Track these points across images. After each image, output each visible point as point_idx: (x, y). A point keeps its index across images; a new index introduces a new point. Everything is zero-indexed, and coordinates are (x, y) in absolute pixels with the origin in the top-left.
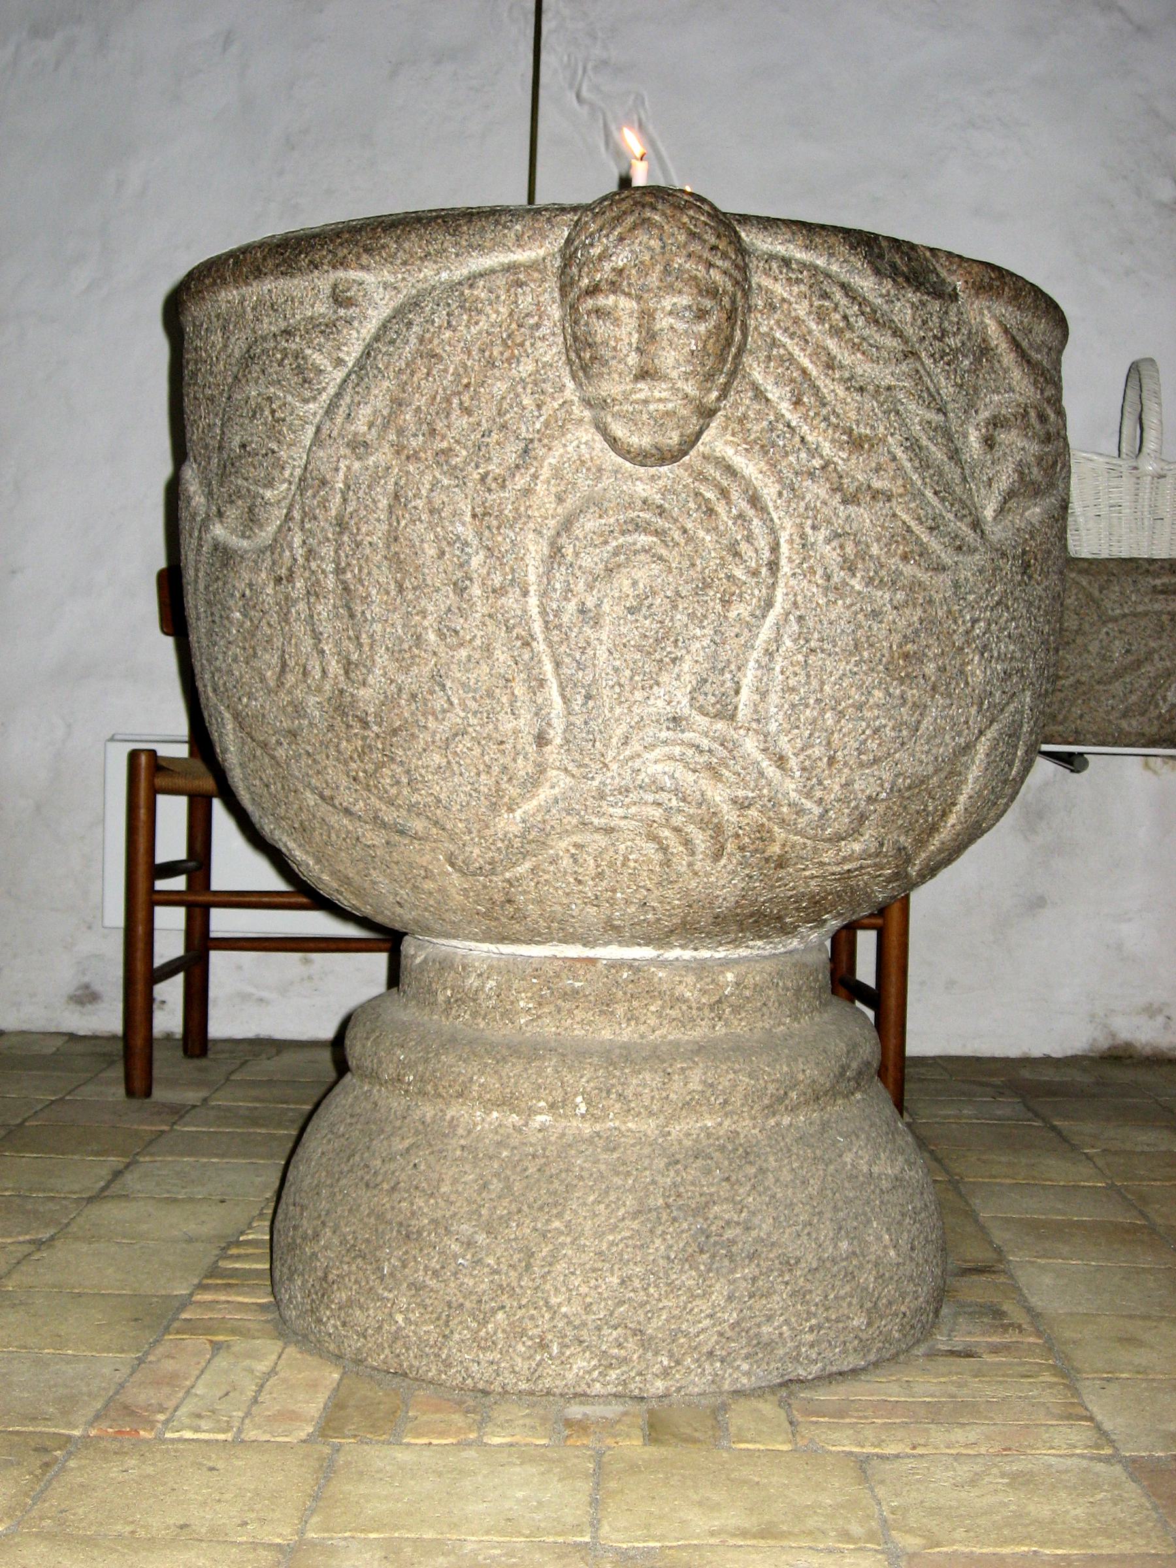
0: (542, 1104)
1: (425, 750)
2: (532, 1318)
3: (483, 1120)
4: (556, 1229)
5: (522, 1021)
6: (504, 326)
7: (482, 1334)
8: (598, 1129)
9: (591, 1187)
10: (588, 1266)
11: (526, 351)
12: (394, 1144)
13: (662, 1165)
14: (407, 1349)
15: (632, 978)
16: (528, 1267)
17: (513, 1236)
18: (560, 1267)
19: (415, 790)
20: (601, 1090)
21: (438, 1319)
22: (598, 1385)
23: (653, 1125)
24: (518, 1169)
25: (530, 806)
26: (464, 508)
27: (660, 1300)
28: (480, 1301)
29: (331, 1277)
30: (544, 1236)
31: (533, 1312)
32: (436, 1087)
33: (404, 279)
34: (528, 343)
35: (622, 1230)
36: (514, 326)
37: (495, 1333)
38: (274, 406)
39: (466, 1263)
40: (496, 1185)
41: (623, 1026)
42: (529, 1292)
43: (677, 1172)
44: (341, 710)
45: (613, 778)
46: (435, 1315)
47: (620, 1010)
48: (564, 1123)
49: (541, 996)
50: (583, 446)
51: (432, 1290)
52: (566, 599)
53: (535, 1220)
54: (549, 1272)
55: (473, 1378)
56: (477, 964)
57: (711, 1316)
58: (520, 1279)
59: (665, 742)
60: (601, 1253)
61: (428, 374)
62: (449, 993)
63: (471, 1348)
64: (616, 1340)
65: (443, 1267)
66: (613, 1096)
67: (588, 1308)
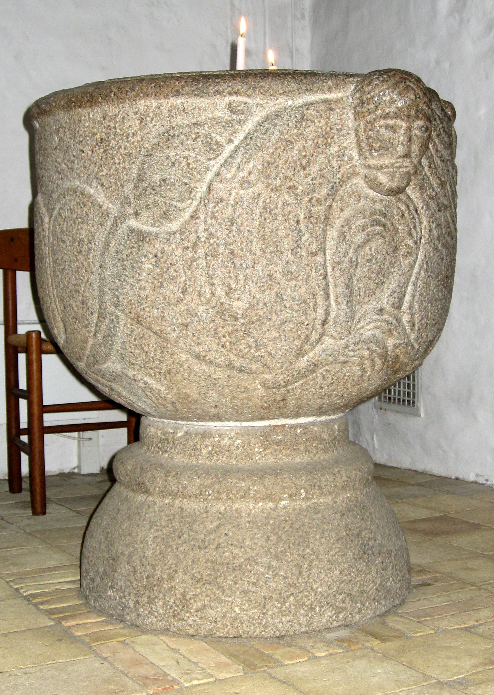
0: (286, 496)
1: (268, 330)
2: (306, 596)
3: (254, 507)
4: (308, 553)
5: (257, 458)
6: (324, 128)
7: (284, 608)
8: (308, 504)
9: (316, 531)
10: (326, 568)
11: (335, 141)
12: (207, 526)
13: (339, 517)
14: (242, 623)
15: (303, 432)
16: (300, 573)
17: (290, 560)
18: (314, 571)
19: (258, 350)
20: (311, 485)
21: (259, 606)
22: (335, 622)
23: (330, 499)
24: (281, 528)
25: (311, 354)
26: (300, 214)
27: (355, 578)
28: (280, 594)
29: (188, 597)
30: (304, 557)
31: (306, 593)
32: (228, 495)
33: (267, 103)
34: (335, 137)
35: (335, 548)
36: (328, 129)
37: (290, 607)
38: (189, 161)
39: (270, 576)
40: (273, 538)
41: (304, 455)
42: (303, 584)
43: (346, 520)
44: (221, 313)
45: (352, 338)
46: (257, 604)
47: (302, 447)
48: (293, 504)
49: (265, 445)
50: (353, 186)
51: (253, 592)
52: (344, 256)
53: (298, 550)
54: (310, 574)
55: (279, 631)
56: (228, 433)
57: (373, 582)
58: (298, 579)
59: (375, 321)
60: (329, 561)
61: (284, 150)
62: (210, 449)
63: (278, 616)
64: (342, 599)
65: (258, 580)
66: (317, 488)
67: (329, 587)
